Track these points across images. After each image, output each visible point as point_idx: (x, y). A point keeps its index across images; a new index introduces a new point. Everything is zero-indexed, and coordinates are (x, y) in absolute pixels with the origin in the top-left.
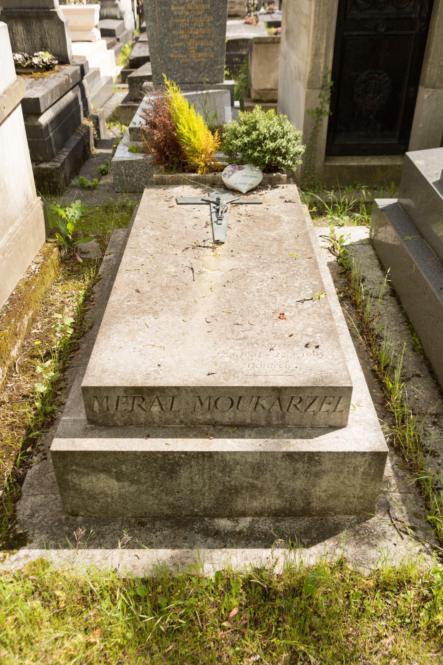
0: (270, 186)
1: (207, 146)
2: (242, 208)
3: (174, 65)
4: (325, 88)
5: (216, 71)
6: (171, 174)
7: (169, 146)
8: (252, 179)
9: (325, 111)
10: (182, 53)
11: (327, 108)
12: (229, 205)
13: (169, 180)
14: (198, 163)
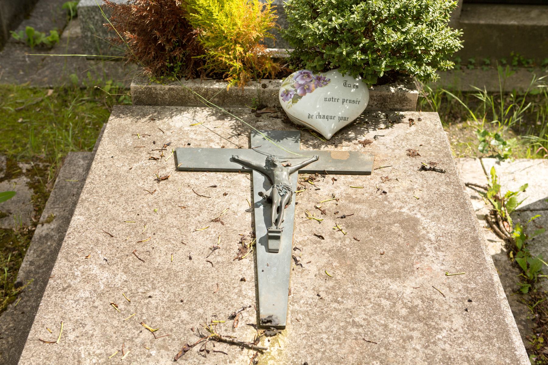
0: (382, 115)
1: (248, 26)
2: (325, 186)
6: (169, 82)
13: (163, 95)
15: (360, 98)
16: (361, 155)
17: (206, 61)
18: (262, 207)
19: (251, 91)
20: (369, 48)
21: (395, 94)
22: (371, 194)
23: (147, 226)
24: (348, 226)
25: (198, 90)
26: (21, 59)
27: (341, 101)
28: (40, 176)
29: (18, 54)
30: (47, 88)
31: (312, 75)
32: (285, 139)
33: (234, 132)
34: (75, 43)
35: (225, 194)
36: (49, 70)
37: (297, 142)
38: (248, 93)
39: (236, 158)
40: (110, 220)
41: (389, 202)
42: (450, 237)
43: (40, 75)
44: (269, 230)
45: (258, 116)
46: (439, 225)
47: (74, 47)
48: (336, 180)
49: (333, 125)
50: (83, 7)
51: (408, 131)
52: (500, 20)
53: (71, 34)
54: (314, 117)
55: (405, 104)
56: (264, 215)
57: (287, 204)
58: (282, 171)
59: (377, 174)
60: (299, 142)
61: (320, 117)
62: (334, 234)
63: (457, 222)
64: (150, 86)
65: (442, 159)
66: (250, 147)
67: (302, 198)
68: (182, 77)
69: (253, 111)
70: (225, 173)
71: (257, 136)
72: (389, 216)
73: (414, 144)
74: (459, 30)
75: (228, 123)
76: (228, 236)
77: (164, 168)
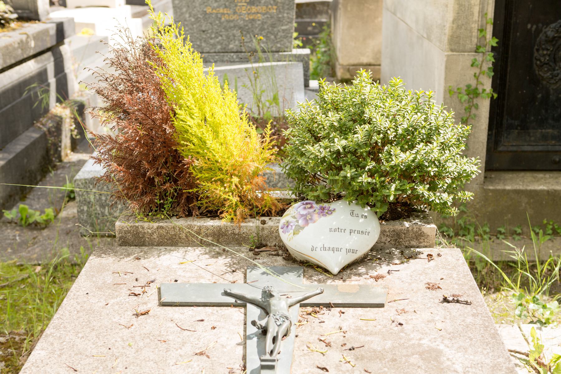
0: (397, 252)
1: (245, 158)
2: (331, 318)
3: (211, 24)
4: (481, 50)
5: (280, 34)
6: (159, 220)
7: (155, 159)
8: (355, 237)
9: (484, 90)
10: (226, 7)
11: (487, 85)
12: (296, 312)
13: (152, 234)
14: (224, 196)
15: (369, 229)
16: (373, 288)
17: (199, 196)
18: (255, 339)
19: (248, 229)
20: (377, 172)
21: (410, 229)
22: (385, 326)
23: (118, 360)
24: (358, 358)
25: (190, 227)
26: (11, 237)
27: (348, 231)
28: (15, 349)
29: (9, 233)
30: (35, 265)
31: (315, 205)
32: (285, 274)
33: (229, 269)
34: (71, 223)
35: (214, 328)
36: (40, 248)
37: (299, 276)
38: (245, 230)
39: (229, 291)
40: (76, 354)
41: (406, 333)
42: (480, 368)
43: (29, 252)
44: (262, 358)
45: (257, 254)
46: (467, 356)
47: (69, 226)
48: (343, 313)
49: (340, 258)
50: (80, 180)
51: (427, 266)
52: (527, 185)
53: (68, 214)
54: (318, 249)
55: (421, 241)
56: (258, 346)
57: (285, 335)
58: (280, 299)
59: (392, 307)
60: (302, 276)
61: (325, 249)
62: (341, 366)
63: (488, 353)
64: (137, 224)
65: (467, 292)
66: (245, 282)
67: (303, 330)
68: (173, 215)
69: (251, 250)
70: (215, 308)
71: (254, 272)
72: (407, 348)
73: (434, 279)
74: (475, 158)
75: (222, 261)
76: (213, 369)
77: (145, 303)
